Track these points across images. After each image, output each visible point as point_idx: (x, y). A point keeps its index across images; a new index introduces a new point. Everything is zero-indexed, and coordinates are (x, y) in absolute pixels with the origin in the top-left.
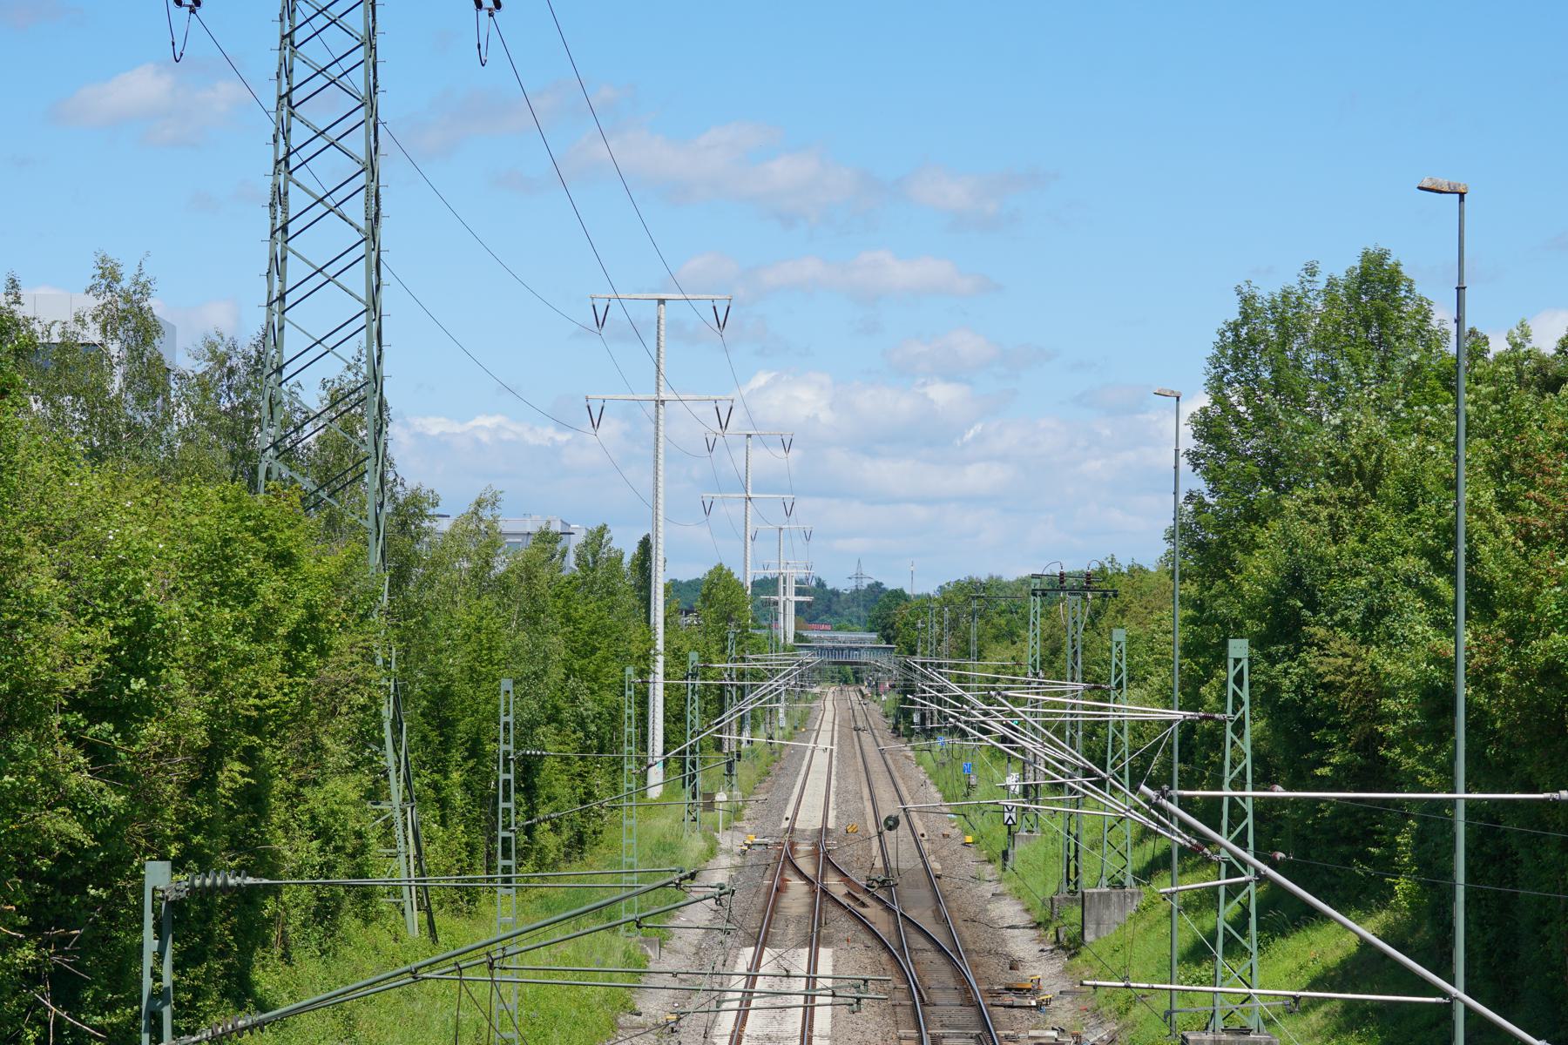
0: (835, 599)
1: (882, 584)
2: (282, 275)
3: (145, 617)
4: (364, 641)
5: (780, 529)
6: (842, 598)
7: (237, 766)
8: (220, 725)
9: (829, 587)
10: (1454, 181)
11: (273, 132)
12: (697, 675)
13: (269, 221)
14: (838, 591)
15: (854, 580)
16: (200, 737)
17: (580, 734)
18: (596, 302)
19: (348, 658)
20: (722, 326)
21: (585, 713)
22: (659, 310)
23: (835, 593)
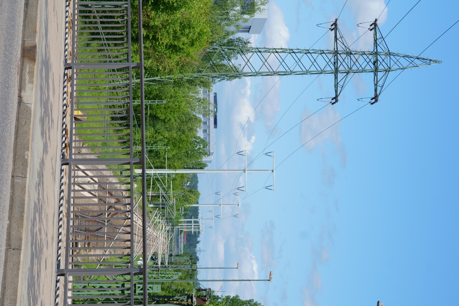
0: (193, 247)
1: (198, 260)
2: (265, 51)
3: (176, 9)
4: (175, 69)
5: (213, 219)
6: (194, 249)
7: (145, 34)
8: (154, 28)
9: (197, 245)
10: (272, 279)
11: (300, 49)
12: (169, 177)
13: (278, 48)
14: (196, 247)
15: (199, 249)
16: (152, 23)
17: (152, 142)
18: (272, 153)
19: (170, 65)
20: (266, 188)
21: (158, 143)
22: (270, 170)
23: (195, 247)
